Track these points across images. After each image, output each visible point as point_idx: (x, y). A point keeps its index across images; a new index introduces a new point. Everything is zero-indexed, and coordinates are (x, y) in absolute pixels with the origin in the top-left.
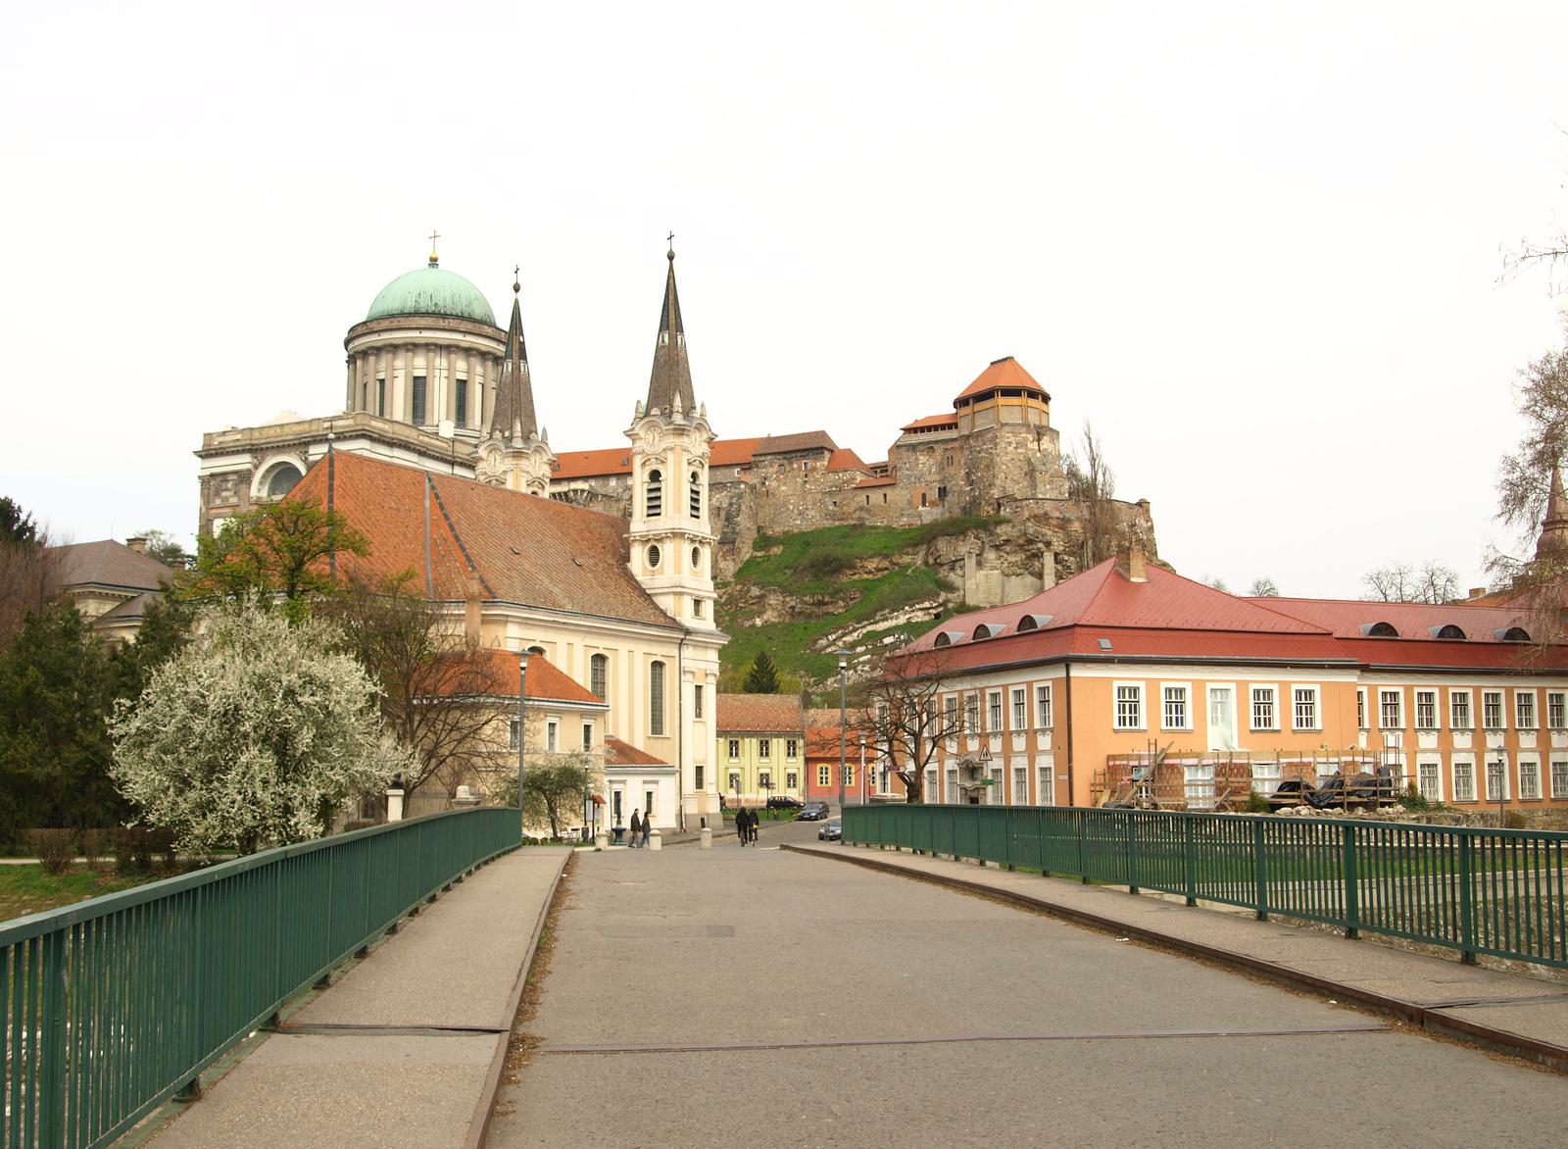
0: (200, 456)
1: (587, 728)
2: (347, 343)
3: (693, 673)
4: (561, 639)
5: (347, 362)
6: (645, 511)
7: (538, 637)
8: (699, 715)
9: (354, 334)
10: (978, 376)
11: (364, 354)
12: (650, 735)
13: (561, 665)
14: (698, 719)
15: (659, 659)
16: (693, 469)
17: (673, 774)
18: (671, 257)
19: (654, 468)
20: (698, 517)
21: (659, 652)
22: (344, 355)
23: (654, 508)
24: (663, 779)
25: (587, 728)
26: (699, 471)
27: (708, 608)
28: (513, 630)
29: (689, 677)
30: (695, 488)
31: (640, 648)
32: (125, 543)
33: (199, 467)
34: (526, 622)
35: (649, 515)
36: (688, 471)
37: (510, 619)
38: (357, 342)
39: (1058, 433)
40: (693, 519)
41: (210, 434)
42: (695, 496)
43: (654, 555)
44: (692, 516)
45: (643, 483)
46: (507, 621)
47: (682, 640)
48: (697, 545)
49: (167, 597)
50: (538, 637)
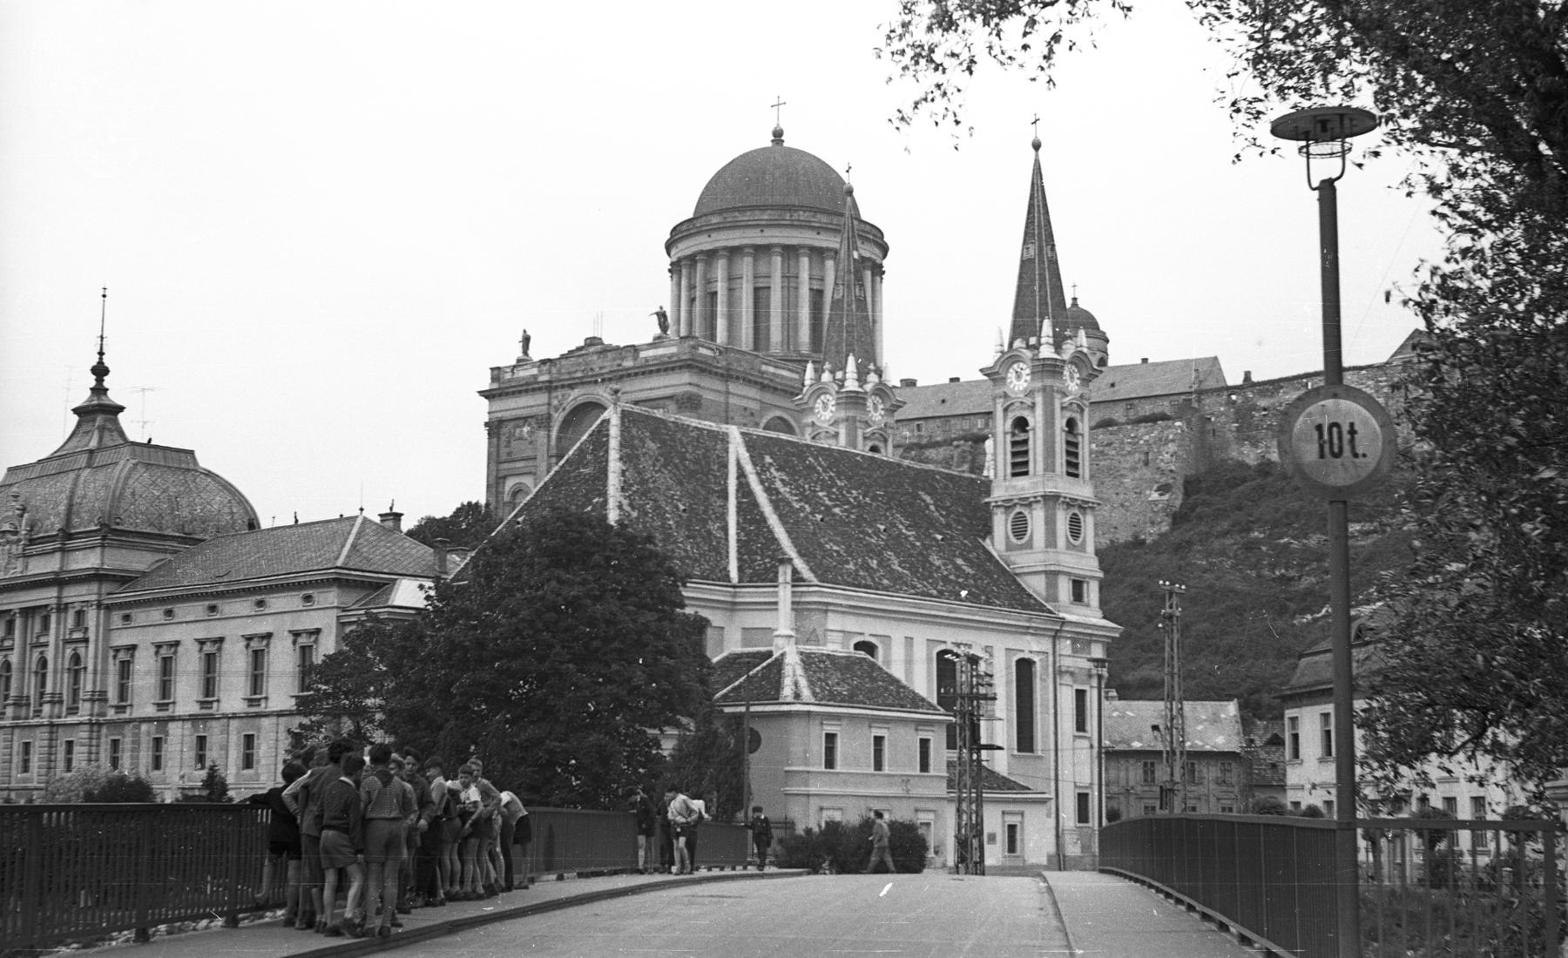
0: (486, 397)
1: (879, 741)
2: (669, 247)
3: (1072, 674)
4: (898, 632)
5: (670, 271)
6: (1009, 471)
7: (869, 629)
8: (1081, 725)
9: (679, 234)
10: (1320, 303)
11: (692, 259)
12: (1016, 752)
13: (898, 671)
14: (1081, 734)
15: (1026, 655)
16: (1068, 414)
17: (1044, 802)
18: (102, 338)
19: (1018, 414)
20: (1076, 476)
21: (1033, 647)
22: (666, 262)
23: (1020, 468)
24: (1029, 811)
25: (879, 741)
26: (1077, 416)
27: (1092, 593)
28: (834, 622)
29: (1067, 679)
30: (1071, 439)
31: (922, 635)
32: (377, 520)
33: (482, 410)
34: (855, 611)
35: (1014, 475)
36: (1062, 417)
37: (831, 608)
38: (681, 246)
39: (191, 453)
40: (1071, 479)
41: (499, 368)
42: (1072, 449)
43: (1020, 527)
44: (1069, 474)
45: (1005, 433)
46: (826, 611)
47: (1057, 631)
48: (1076, 511)
49: (1218, 648)
50: (869, 629)
